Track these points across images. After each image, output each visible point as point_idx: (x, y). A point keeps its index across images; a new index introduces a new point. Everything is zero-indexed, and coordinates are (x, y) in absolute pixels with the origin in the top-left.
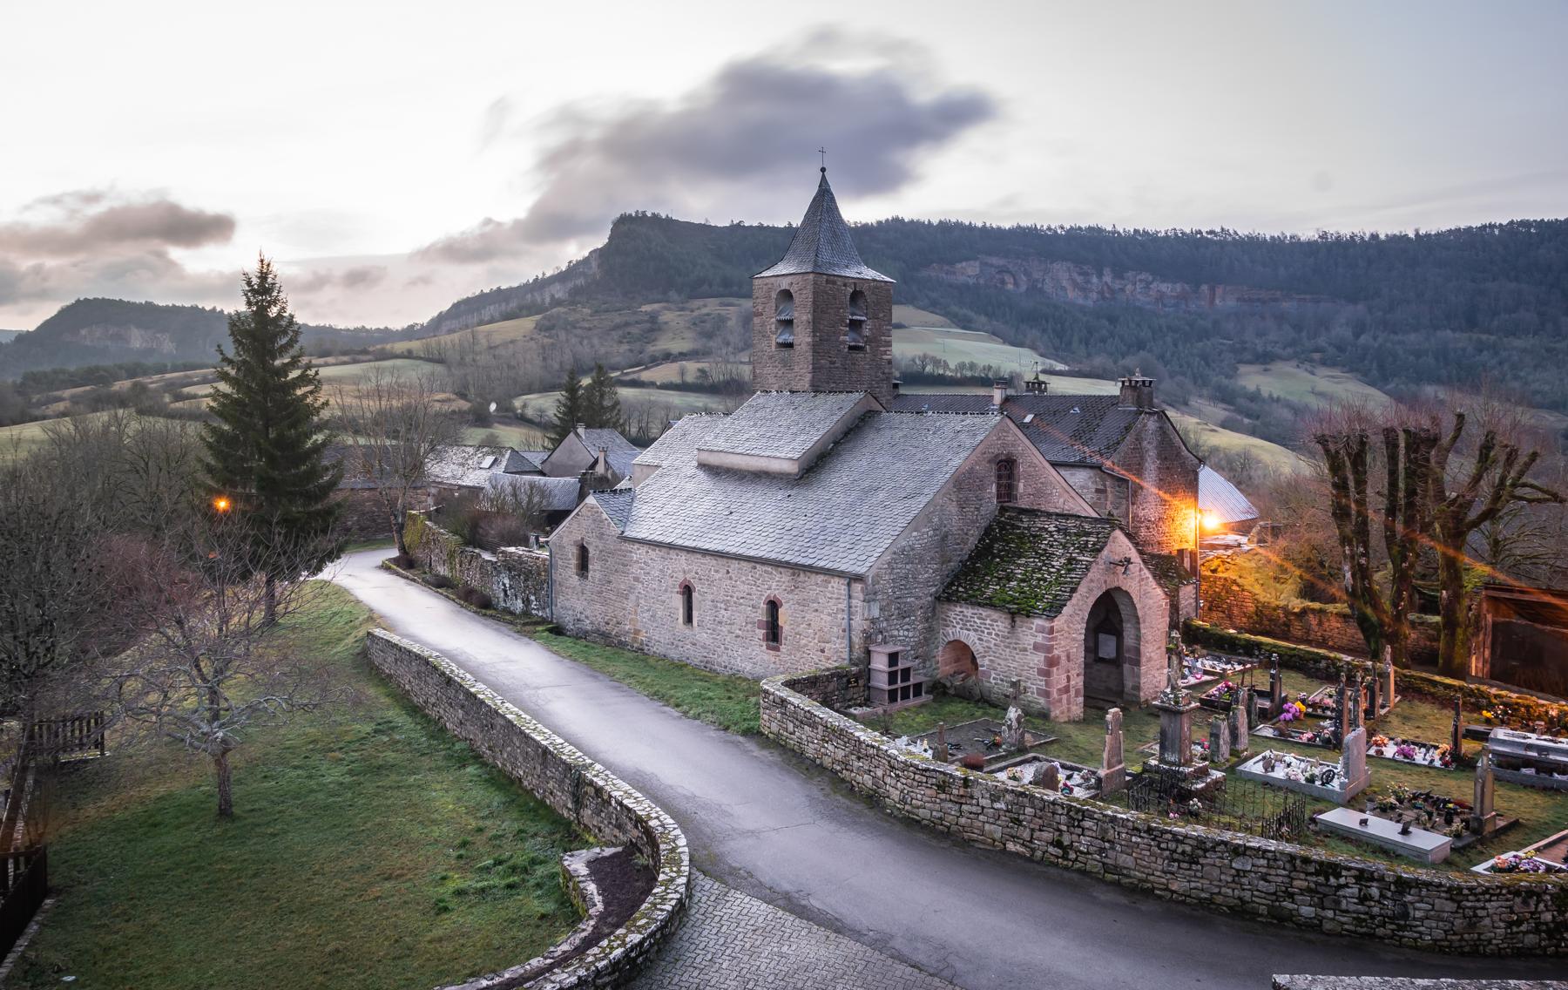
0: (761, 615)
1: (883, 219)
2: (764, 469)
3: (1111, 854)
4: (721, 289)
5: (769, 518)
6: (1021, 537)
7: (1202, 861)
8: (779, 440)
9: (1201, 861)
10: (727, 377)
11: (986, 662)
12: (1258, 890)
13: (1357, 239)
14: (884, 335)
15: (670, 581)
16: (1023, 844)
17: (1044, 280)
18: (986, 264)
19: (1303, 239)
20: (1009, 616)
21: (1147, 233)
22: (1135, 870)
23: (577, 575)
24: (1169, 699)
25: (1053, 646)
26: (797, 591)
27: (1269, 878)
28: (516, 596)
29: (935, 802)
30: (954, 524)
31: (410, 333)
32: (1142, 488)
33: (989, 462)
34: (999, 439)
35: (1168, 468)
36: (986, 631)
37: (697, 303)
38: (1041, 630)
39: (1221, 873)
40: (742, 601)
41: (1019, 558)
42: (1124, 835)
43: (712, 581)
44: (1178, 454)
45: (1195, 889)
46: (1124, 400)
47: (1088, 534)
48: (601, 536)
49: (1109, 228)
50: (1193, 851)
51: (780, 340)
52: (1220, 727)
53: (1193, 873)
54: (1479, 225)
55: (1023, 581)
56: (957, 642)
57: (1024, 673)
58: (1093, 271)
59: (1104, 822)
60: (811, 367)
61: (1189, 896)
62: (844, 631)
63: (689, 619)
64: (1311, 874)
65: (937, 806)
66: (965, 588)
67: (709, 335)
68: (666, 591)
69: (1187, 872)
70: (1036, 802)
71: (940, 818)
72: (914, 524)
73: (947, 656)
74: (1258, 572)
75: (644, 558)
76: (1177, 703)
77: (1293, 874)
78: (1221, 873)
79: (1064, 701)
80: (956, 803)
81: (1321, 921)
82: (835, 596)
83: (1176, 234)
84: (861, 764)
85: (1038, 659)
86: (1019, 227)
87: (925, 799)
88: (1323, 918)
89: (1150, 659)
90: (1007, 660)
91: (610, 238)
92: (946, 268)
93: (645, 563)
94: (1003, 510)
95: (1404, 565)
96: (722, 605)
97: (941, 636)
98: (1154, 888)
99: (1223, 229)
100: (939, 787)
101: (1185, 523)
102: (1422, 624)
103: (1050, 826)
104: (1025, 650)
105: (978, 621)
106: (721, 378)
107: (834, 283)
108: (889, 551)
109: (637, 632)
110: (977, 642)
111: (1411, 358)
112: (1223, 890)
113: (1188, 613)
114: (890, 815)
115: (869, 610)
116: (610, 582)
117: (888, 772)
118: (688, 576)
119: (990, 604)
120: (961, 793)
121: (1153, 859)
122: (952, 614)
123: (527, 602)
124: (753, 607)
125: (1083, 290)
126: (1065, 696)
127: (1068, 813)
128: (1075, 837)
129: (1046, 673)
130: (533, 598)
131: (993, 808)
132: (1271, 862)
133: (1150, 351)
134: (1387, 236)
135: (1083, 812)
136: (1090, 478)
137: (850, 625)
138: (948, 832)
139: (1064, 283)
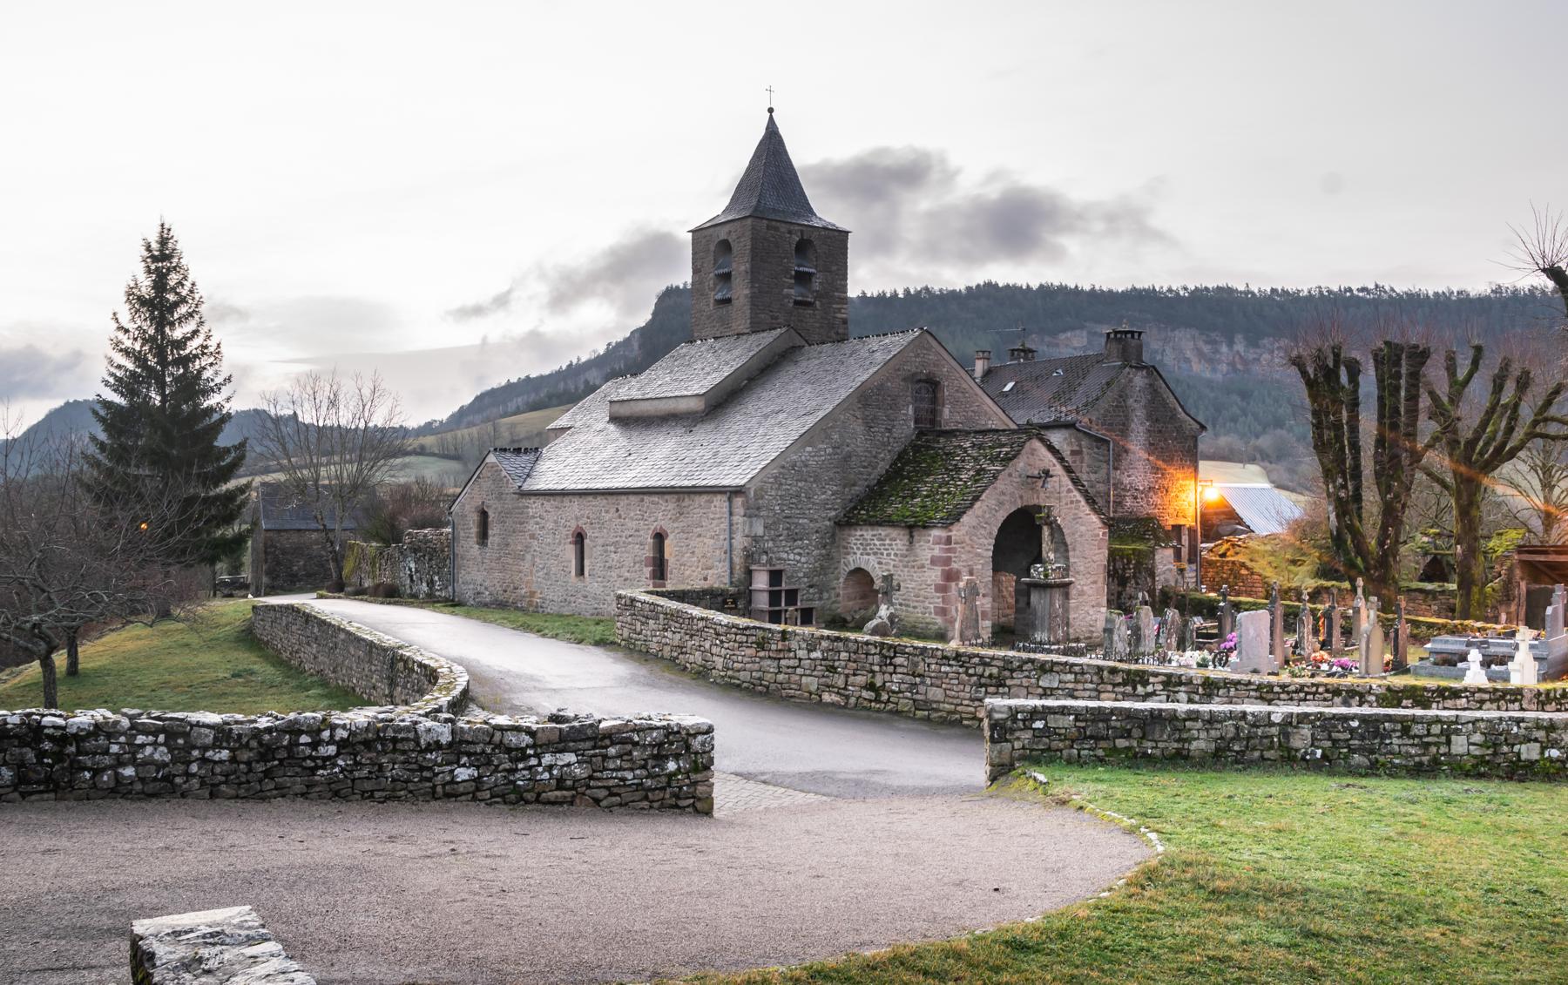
0: (648, 552)
3: (922, 689)
7: (1009, 682)
8: (692, 380)
13: (1537, 293)
14: (837, 290)
15: (564, 531)
16: (838, 693)
17: (1164, 350)
18: (1095, 333)
19: (1472, 294)
20: (907, 531)
21: (1287, 292)
22: (944, 702)
23: (478, 544)
24: (1039, 573)
25: (950, 558)
27: (1076, 693)
28: (421, 579)
29: (755, 662)
31: (428, 429)
32: (1126, 451)
33: (904, 380)
34: (917, 356)
35: (1160, 431)
36: (885, 552)
40: (630, 539)
41: (928, 476)
44: (1173, 417)
46: (1108, 355)
47: (1004, 446)
48: (500, 496)
49: (1242, 288)
50: (999, 673)
51: (719, 296)
52: (1114, 621)
55: (927, 496)
57: (922, 592)
58: (1222, 339)
59: (915, 655)
60: (749, 321)
62: (725, 553)
63: (581, 571)
65: (756, 666)
68: (560, 543)
70: (850, 644)
71: (760, 679)
75: (540, 511)
76: (1046, 576)
77: (1099, 688)
80: (775, 659)
82: (717, 516)
83: (1321, 292)
85: (935, 575)
86: (1134, 289)
87: (746, 659)
89: (1082, 593)
91: (655, 314)
92: (1047, 339)
94: (921, 434)
95: (1389, 496)
96: (612, 548)
97: (842, 566)
98: (962, 718)
99: (1377, 286)
100: (758, 644)
101: (1183, 496)
102: (1443, 592)
103: (863, 668)
105: (877, 543)
109: (532, 594)
110: (877, 566)
113: (1166, 580)
114: (712, 683)
115: (751, 526)
116: (507, 545)
118: (580, 523)
120: (780, 647)
121: (962, 687)
123: (431, 583)
125: (1211, 361)
128: (887, 677)
131: (809, 659)
132: (1079, 677)
133: (1290, 430)
135: (895, 647)
136: (1065, 439)
137: (731, 545)
138: (767, 692)
139: (1189, 354)
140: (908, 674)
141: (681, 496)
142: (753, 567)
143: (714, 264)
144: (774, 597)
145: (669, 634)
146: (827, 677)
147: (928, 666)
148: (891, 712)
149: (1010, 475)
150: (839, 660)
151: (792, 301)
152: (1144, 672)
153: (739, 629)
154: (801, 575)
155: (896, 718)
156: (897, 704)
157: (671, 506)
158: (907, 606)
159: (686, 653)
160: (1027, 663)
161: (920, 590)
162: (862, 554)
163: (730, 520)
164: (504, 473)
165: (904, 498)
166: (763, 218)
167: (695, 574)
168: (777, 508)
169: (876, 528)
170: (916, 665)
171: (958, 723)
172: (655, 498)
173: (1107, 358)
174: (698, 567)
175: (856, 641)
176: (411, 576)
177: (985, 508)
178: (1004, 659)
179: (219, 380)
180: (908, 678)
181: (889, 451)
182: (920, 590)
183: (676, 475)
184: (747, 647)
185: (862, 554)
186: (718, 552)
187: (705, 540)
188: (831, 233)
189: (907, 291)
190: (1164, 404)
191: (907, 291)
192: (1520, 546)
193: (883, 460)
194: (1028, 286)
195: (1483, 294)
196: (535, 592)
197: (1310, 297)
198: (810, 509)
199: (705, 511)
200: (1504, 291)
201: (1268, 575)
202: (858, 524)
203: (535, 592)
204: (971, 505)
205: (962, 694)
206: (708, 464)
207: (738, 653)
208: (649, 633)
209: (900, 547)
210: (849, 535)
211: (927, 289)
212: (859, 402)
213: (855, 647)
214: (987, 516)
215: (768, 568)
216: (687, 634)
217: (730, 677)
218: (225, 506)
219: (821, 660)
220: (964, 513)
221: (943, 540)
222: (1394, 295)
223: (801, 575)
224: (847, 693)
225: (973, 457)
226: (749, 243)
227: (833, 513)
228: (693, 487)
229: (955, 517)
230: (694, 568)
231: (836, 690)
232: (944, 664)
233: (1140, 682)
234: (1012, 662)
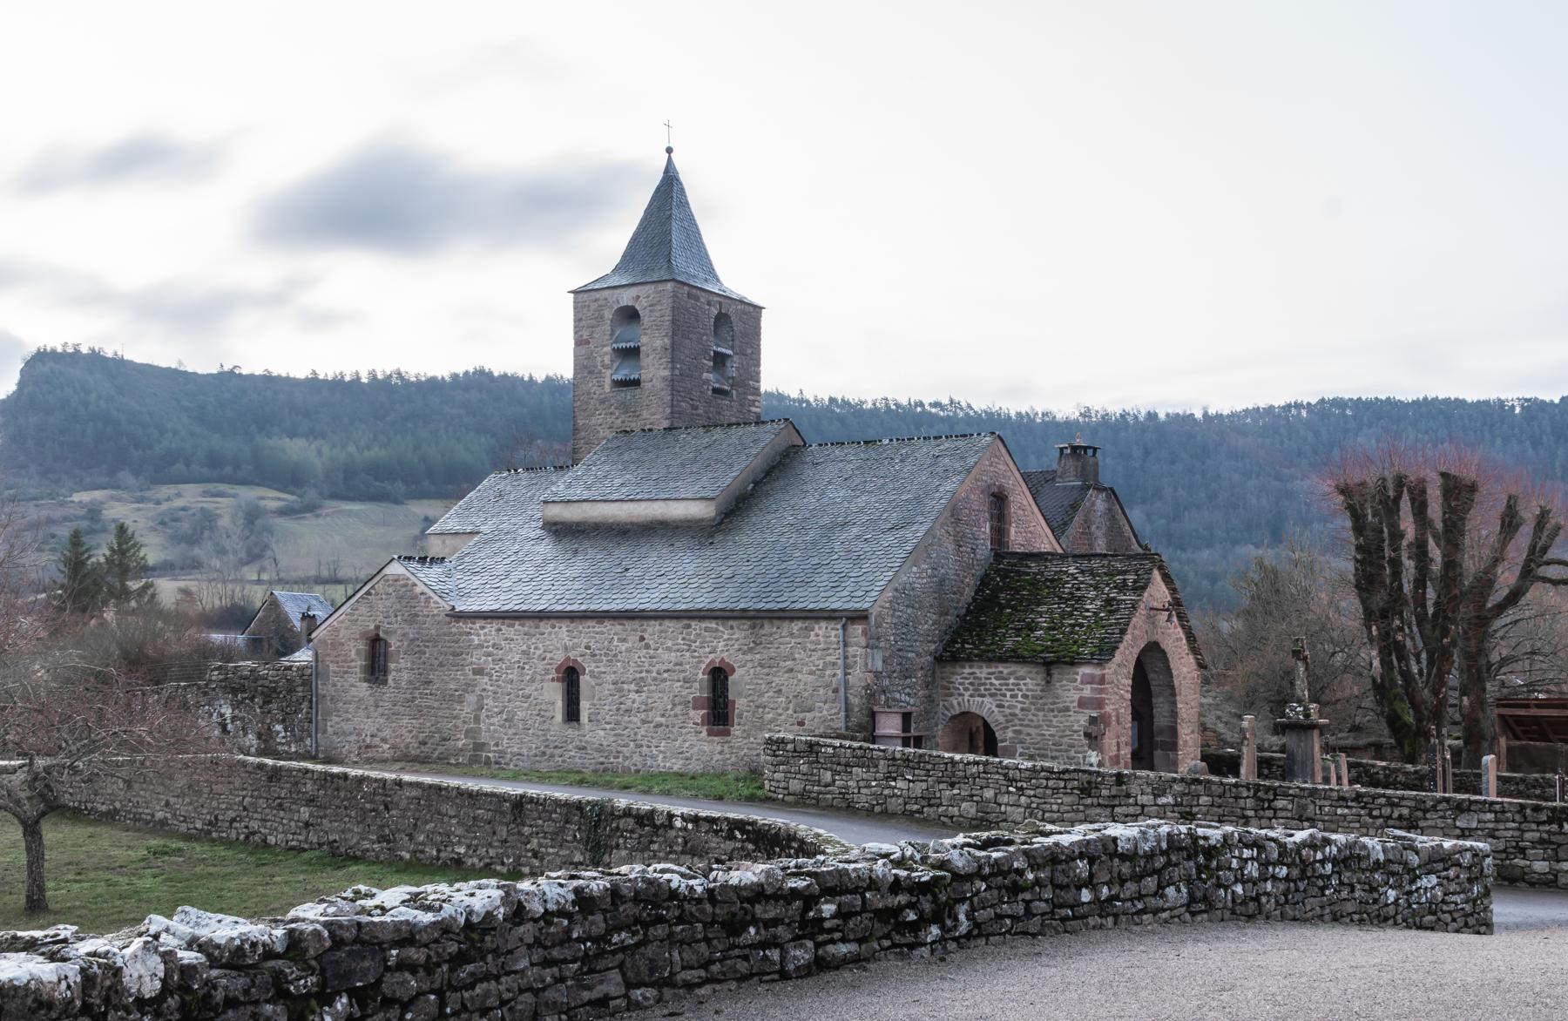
0: (699, 687)
1: (460, 371)
2: (660, 518)
4: (205, 470)
5: (691, 569)
6: (1034, 583)
10: (227, 602)
11: (1010, 734)
13: (1129, 419)
15: (541, 666)
19: (1060, 416)
20: (1043, 669)
24: (1297, 713)
26: (759, 648)
30: (950, 568)
36: (1008, 694)
37: (165, 491)
38: (1090, 680)
40: (665, 675)
42: (1326, 809)
43: (615, 655)
49: (795, 395)
50: (1411, 814)
51: (618, 377)
54: (1282, 404)
56: (965, 714)
63: (572, 714)
64: (1543, 823)
66: (973, 643)
67: (193, 540)
68: (532, 680)
70: (1214, 788)
72: (912, 557)
73: (946, 739)
80: (1106, 806)
81: (1556, 876)
82: (821, 646)
83: (887, 405)
84: (956, 792)
88: (1558, 871)
90: (1040, 726)
91: (21, 384)
93: (494, 646)
96: (633, 687)
99: (952, 401)
100: (1082, 790)
103: (1232, 814)
105: (997, 682)
106: (217, 603)
107: (697, 299)
108: (891, 586)
110: (996, 710)
111: (1205, 583)
117: (1004, 789)
118: (572, 655)
119: (1015, 657)
120: (1114, 792)
124: (686, 681)
127: (1255, 794)
130: (279, 727)
132: (1499, 815)
134: (1168, 415)
135: (1275, 789)
140: (1293, 819)
141: (758, 622)
142: (876, 708)
150: (1198, 805)
151: (710, 388)
162: (971, 696)
163: (845, 652)
164: (420, 588)
169: (994, 664)
170: (1304, 808)
173: (1060, 477)
174: (788, 709)
176: (224, 727)
178: (1415, 799)
184: (1065, 794)
186: (822, 691)
189: (373, 375)
190: (1121, 532)
191: (373, 375)
192: (1499, 700)
193: (968, 585)
194: (531, 377)
197: (874, 411)
198: (916, 641)
199: (799, 640)
200: (1093, 415)
202: (969, 660)
209: (1030, 687)
211: (399, 373)
212: (952, 516)
219: (1173, 806)
222: (972, 413)
230: (780, 711)
232: (1340, 807)
234: (1424, 802)
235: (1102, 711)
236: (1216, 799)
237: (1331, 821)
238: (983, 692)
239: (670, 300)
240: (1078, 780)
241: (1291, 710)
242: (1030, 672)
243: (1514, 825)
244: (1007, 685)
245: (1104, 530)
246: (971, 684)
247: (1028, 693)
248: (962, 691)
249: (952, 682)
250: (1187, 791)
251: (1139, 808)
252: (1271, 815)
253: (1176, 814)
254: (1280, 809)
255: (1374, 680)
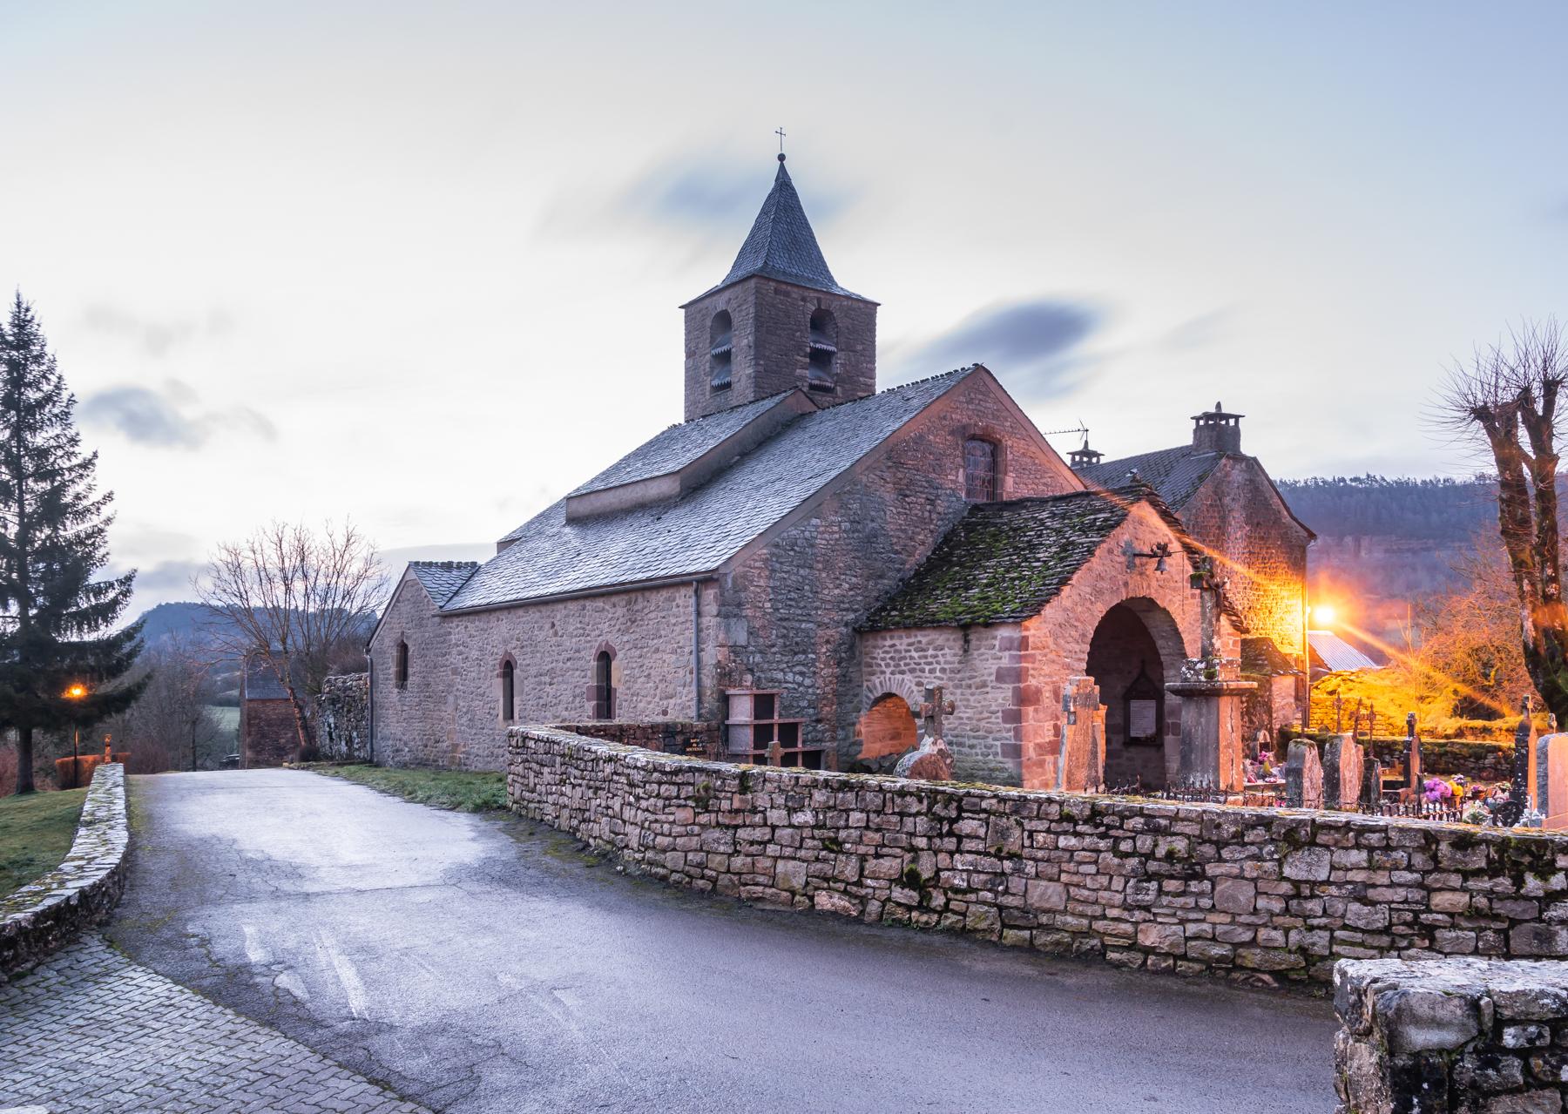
9: (1211, 869)
12: (1345, 927)
14: (863, 375)
16: (845, 892)
20: (960, 634)
21: (1285, 483)
22: (1065, 912)
23: (397, 687)
24: (1197, 673)
27: (1371, 893)
28: (340, 737)
35: (1262, 538)
36: (927, 668)
38: (1008, 645)
39: (1258, 893)
44: (1277, 521)
45: (1196, 938)
47: (1100, 511)
50: (1191, 850)
51: (716, 382)
52: (1304, 756)
53: (1191, 901)
55: (987, 585)
57: (983, 724)
59: (1001, 815)
61: (1184, 957)
62: (691, 673)
64: (1478, 873)
69: (1181, 901)
70: (869, 796)
74: (1394, 691)
76: (1211, 676)
77: (1430, 880)
78: (1258, 893)
79: (1050, 767)
80: (727, 827)
82: (681, 619)
83: (1316, 483)
85: (1002, 696)
87: (677, 829)
96: (547, 679)
99: (1368, 476)
100: (697, 799)
103: (895, 843)
104: (984, 685)
105: (915, 655)
109: (456, 746)
110: (915, 688)
112: (1263, 934)
119: (935, 624)
120: (736, 805)
121: (1104, 880)
122: (879, 653)
123: (350, 742)
126: (1049, 758)
127: (930, 809)
128: (943, 860)
129: (1014, 717)
131: (791, 826)
132: (1377, 856)
135: (960, 800)
137: (699, 661)
140: (987, 854)
141: (633, 596)
142: (731, 691)
143: (711, 343)
144: (762, 735)
145: (567, 789)
146: (825, 860)
147: (1031, 836)
148: (950, 931)
149: (1110, 551)
150: (847, 827)
152: (1542, 844)
153: (664, 773)
154: (805, 703)
155: (963, 944)
156: (964, 915)
157: (620, 611)
158: (961, 744)
159: (590, 821)
160: (1254, 827)
161: (979, 720)
162: (892, 673)
163: (698, 624)
165: (954, 590)
166: (769, 279)
167: (651, 706)
168: (768, 605)
169: (913, 632)
170: (1003, 834)
171: (1096, 958)
172: (599, 603)
175: (881, 789)
176: (330, 734)
177: (1077, 598)
178: (1200, 818)
179: (95, 497)
180: (987, 863)
181: (931, 532)
182: (979, 720)
183: (629, 569)
184: (679, 806)
185: (893, 673)
186: (681, 673)
187: (665, 657)
188: (855, 305)
193: (923, 543)
195: (1468, 481)
196: (457, 745)
198: (817, 608)
201: (1392, 714)
202: (886, 629)
203: (457, 745)
204: (1057, 592)
205: (1106, 894)
206: (673, 551)
207: (663, 817)
208: (544, 790)
209: (949, 658)
210: (875, 647)
212: (889, 458)
213: (879, 801)
214: (1080, 609)
215: (755, 691)
216: (590, 788)
217: (650, 863)
218: (108, 655)
219: (813, 827)
220: (1048, 602)
221: (1016, 644)
222: (1384, 484)
223: (805, 703)
224: (863, 892)
225: (1055, 530)
226: (752, 310)
227: (852, 616)
228: (648, 579)
229: (1035, 607)
230: (649, 699)
231: (841, 886)
232: (1065, 833)
233: (1531, 867)
234: (1218, 826)
235: (1022, 685)
236: (872, 816)
237: (1048, 861)
238: (904, 668)
239: (753, 297)
240: (693, 784)
241: (1189, 669)
242: (948, 640)
243: (1409, 877)
244: (926, 657)
245: (1242, 502)
246: (891, 658)
247: (946, 666)
248: (884, 668)
249: (875, 658)
250: (831, 803)
251: (768, 830)
252: (953, 847)
253: (816, 842)
254: (968, 836)
255: (1526, 646)
